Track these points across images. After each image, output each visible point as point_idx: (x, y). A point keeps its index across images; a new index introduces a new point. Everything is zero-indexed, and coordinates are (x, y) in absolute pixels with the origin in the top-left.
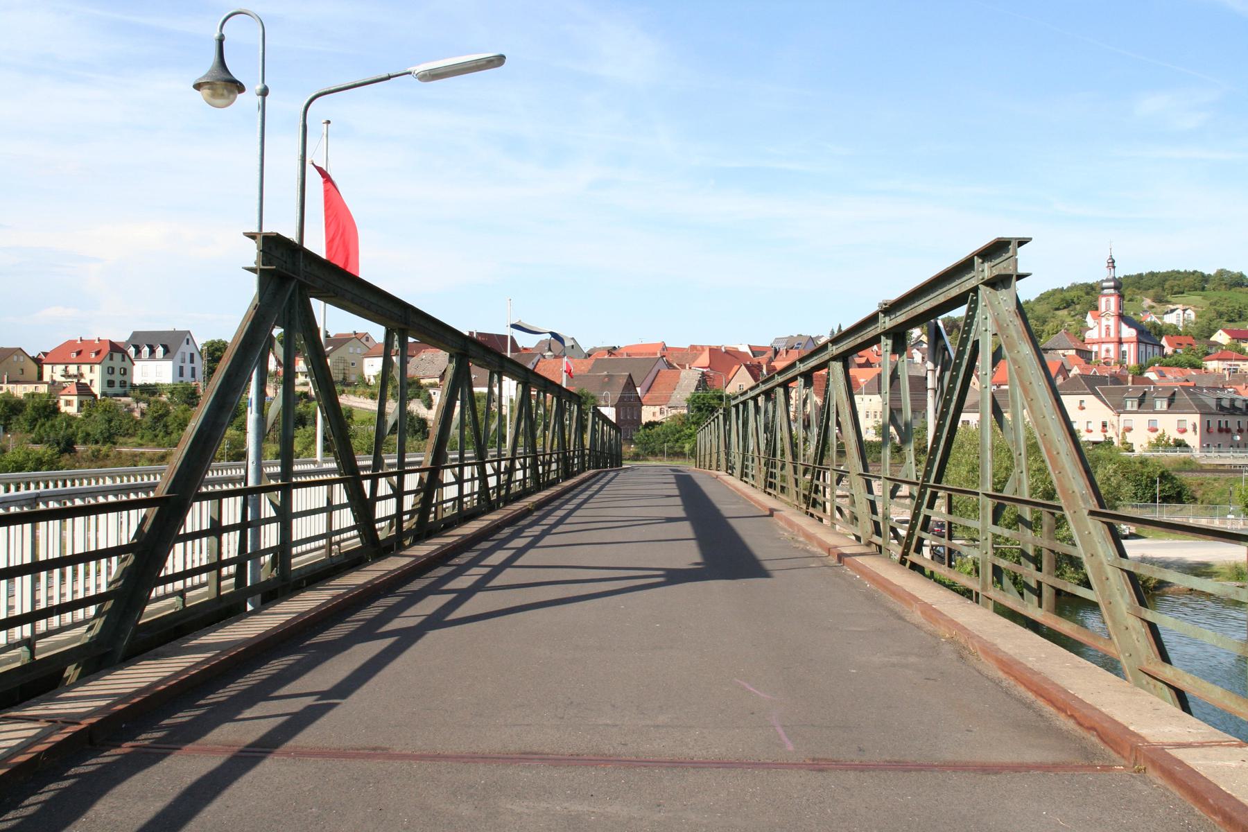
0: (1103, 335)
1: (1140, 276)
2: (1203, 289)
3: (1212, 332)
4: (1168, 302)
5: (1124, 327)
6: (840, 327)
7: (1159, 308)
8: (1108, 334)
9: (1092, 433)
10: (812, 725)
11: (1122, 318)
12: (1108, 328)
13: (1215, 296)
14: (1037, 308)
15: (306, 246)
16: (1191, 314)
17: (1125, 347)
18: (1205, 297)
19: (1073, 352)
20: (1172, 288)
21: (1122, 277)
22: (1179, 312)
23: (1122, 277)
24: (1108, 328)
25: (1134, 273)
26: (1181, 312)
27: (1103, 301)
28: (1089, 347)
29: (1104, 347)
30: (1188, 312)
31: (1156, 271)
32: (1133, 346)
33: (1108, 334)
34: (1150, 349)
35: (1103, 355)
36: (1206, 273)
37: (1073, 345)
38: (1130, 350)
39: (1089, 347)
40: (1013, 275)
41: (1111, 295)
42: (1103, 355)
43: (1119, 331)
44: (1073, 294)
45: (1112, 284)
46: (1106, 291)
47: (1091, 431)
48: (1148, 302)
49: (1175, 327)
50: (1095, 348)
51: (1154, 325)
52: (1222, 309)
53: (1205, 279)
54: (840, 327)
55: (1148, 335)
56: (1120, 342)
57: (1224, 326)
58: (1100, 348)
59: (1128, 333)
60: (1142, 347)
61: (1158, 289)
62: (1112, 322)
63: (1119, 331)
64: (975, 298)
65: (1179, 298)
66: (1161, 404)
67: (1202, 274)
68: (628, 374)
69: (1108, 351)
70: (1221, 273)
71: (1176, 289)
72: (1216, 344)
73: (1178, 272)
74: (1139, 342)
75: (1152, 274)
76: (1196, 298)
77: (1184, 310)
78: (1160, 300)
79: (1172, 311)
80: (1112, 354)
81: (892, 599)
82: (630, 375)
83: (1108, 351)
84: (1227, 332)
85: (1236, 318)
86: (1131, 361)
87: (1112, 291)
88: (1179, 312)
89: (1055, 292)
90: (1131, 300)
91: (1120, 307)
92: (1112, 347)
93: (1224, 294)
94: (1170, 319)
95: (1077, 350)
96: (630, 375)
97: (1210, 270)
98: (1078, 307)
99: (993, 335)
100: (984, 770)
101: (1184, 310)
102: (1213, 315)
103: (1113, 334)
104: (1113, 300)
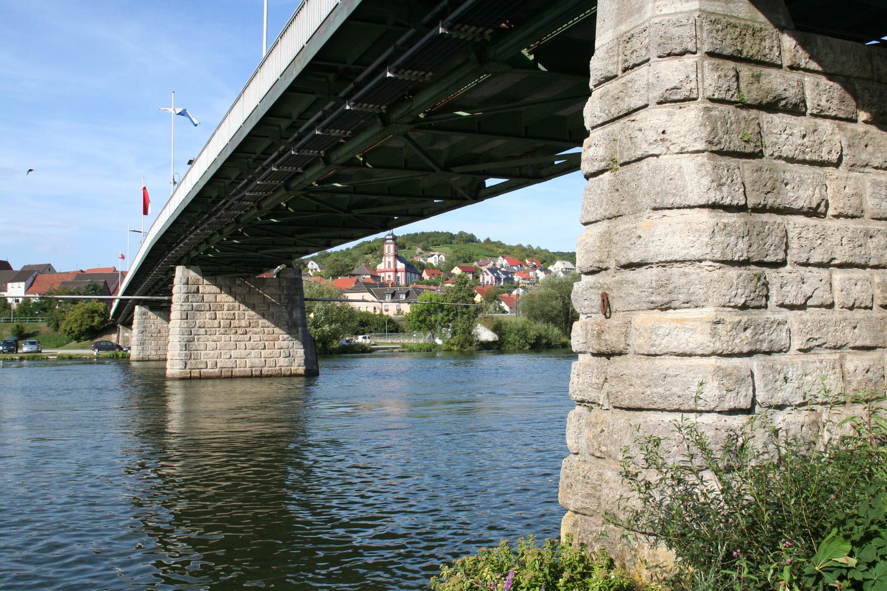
0: (387, 267)
1: (416, 234)
2: (451, 243)
3: (453, 268)
4: (431, 250)
5: (398, 262)
7: (425, 254)
8: (389, 266)
9: (124, 254)
11: (397, 257)
12: (389, 263)
13: (456, 247)
14: (354, 252)
16: (443, 258)
17: (399, 274)
18: (451, 248)
19: (369, 276)
20: (433, 241)
22: (436, 256)
24: (389, 263)
25: (413, 233)
26: (437, 256)
27: (387, 246)
29: (387, 274)
30: (441, 256)
31: (425, 231)
32: (403, 274)
33: (389, 266)
34: (413, 275)
35: (387, 279)
36: (454, 233)
37: (368, 272)
38: (401, 275)
41: (391, 243)
42: (387, 279)
43: (395, 265)
44: (375, 244)
45: (391, 237)
46: (388, 241)
47: (122, 255)
48: (419, 250)
49: (432, 265)
50: (382, 275)
51: (420, 264)
52: (460, 255)
53: (451, 237)
55: (411, 268)
56: (396, 271)
57: (461, 265)
58: (385, 275)
59: (401, 266)
60: (409, 274)
61: (425, 243)
62: (391, 259)
63: (395, 265)
64: (425, 275)
65: (437, 248)
66: (403, 297)
67: (451, 234)
70: (461, 234)
71: (435, 243)
72: (454, 274)
73: (438, 233)
74: (406, 271)
75: (423, 233)
76: (447, 249)
77: (439, 255)
78: (426, 249)
79: (432, 255)
80: (392, 278)
84: (460, 267)
85: (468, 260)
86: (402, 282)
87: (391, 241)
88: (436, 256)
90: (409, 249)
91: (395, 251)
92: (391, 274)
93: (462, 246)
94: (431, 260)
97: (455, 232)
98: (378, 252)
99: (786, 382)
100: (64, 358)
101: (439, 255)
102: (454, 258)
103: (392, 267)
104: (392, 246)
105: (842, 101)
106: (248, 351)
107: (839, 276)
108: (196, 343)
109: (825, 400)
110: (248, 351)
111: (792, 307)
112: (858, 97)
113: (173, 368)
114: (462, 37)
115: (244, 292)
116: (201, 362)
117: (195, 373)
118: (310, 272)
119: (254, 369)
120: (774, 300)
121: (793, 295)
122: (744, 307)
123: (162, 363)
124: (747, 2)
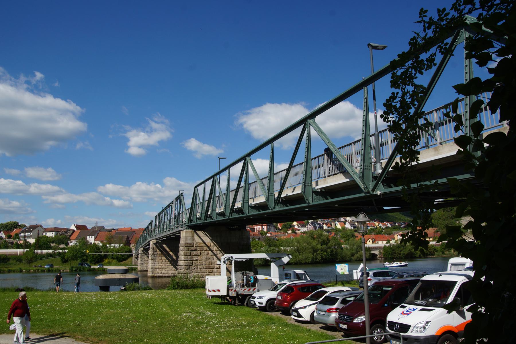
6: (456, 92)
10: (275, 259)
15: (190, 207)
21: (480, 4)
23: (480, 4)
28: (358, 255)
34: (271, 227)
35: (258, 229)
39: (254, 227)
40: (270, 275)
54: (456, 92)
58: (257, 227)
60: (268, 227)
68: (127, 235)
69: (259, 228)
81: (330, 285)
82: (128, 236)
83: (259, 228)
89: (13, 249)
95: (250, 228)
96: (128, 236)
105: (404, 254)
106: (171, 269)
107: (199, 266)
108: (303, 259)
109: (190, 274)
110: (171, 269)
111: (193, 269)
112: (349, 282)
113: (150, 274)
114: (183, 292)
115: (402, 252)
116: (157, 272)
117: (156, 275)
118: (408, 201)
119: (173, 274)
120: (191, 269)
121: (193, 268)
122: (187, 269)
123: (145, 273)
124: (1, 335)
